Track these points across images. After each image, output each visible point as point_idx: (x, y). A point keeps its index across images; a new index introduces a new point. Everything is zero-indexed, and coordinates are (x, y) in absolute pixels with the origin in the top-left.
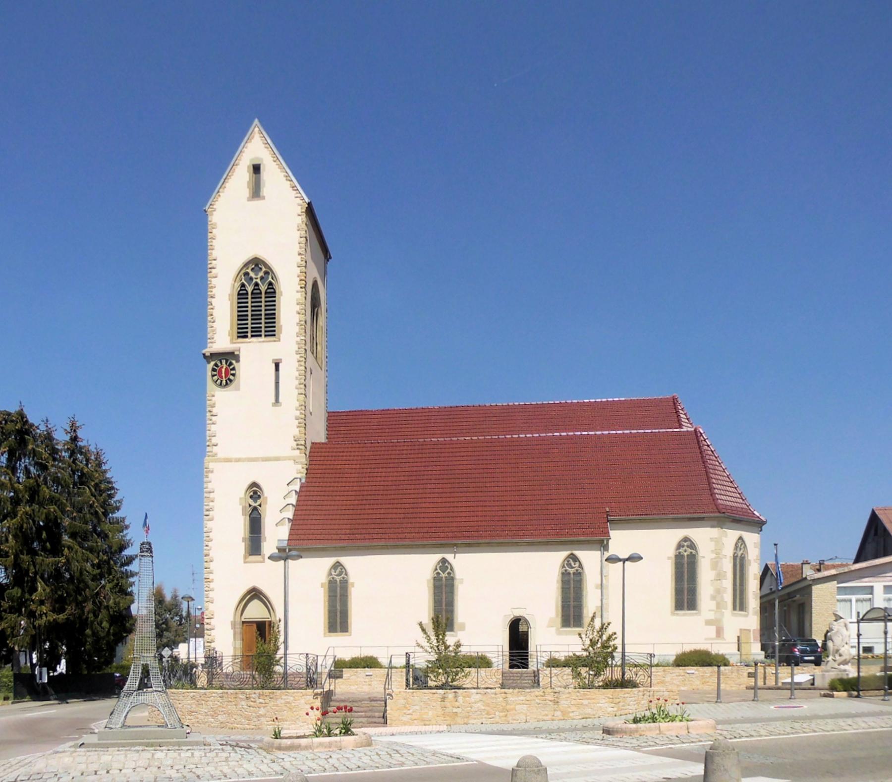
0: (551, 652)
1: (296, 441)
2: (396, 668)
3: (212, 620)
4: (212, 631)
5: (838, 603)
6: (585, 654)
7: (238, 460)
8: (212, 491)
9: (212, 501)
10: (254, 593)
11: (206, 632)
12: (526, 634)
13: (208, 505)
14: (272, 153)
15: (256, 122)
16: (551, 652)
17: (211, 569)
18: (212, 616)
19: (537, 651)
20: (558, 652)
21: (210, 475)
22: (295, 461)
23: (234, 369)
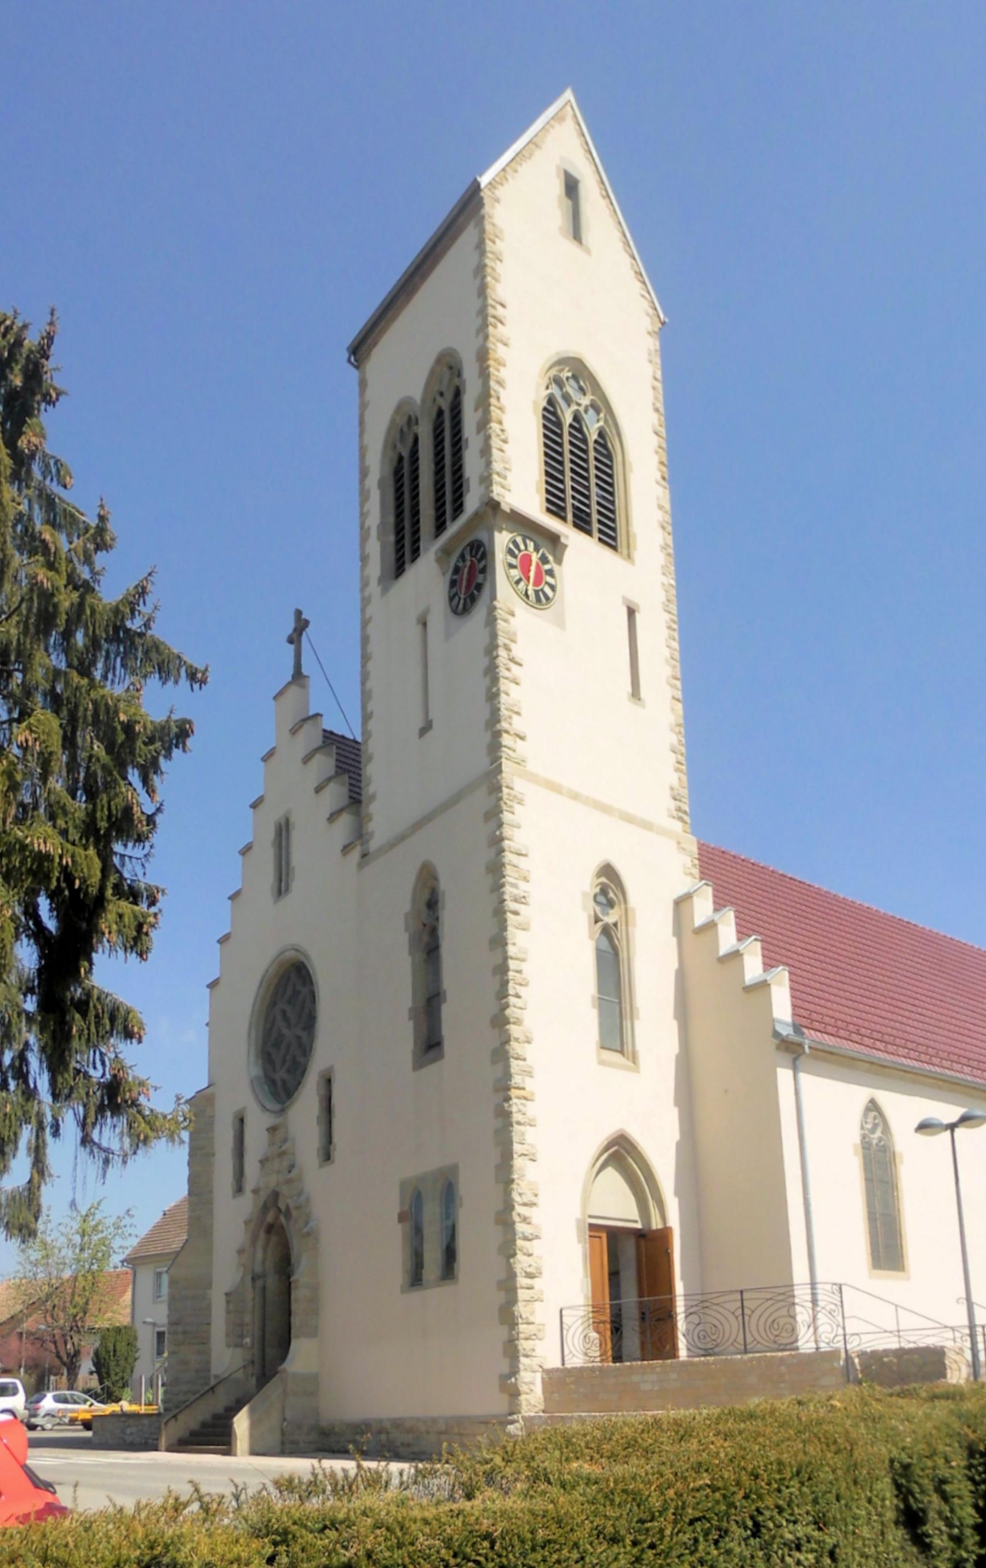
0: (742, 1292)
1: (675, 799)
2: (75, 1491)
3: (534, 1209)
4: (535, 1242)
5: (980, 1380)
6: (130, 1079)
7: (575, 796)
8: (524, 852)
9: (526, 879)
10: (615, 1148)
11: (520, 1243)
12: (512, 510)
13: (515, 886)
14: (604, 193)
15: (568, 95)
16: (742, 1292)
17: (528, 1062)
18: (534, 1200)
19: (899, 1331)
20: (857, 1334)
21: (517, 808)
22: (679, 843)
23: (550, 573)
